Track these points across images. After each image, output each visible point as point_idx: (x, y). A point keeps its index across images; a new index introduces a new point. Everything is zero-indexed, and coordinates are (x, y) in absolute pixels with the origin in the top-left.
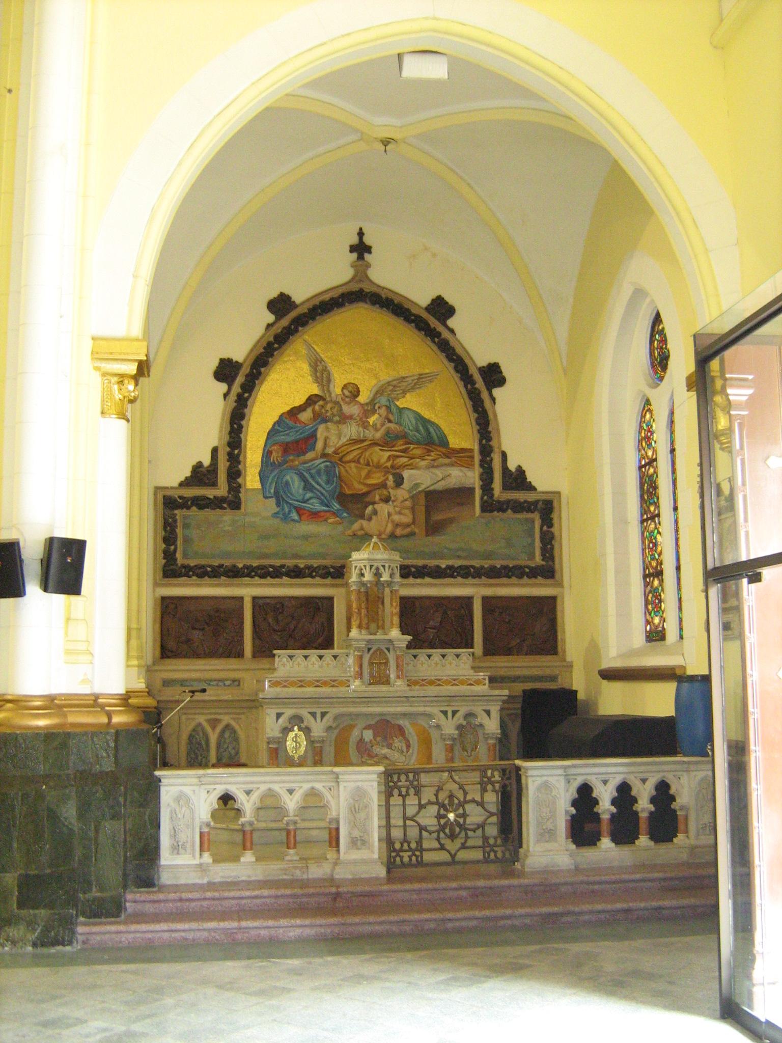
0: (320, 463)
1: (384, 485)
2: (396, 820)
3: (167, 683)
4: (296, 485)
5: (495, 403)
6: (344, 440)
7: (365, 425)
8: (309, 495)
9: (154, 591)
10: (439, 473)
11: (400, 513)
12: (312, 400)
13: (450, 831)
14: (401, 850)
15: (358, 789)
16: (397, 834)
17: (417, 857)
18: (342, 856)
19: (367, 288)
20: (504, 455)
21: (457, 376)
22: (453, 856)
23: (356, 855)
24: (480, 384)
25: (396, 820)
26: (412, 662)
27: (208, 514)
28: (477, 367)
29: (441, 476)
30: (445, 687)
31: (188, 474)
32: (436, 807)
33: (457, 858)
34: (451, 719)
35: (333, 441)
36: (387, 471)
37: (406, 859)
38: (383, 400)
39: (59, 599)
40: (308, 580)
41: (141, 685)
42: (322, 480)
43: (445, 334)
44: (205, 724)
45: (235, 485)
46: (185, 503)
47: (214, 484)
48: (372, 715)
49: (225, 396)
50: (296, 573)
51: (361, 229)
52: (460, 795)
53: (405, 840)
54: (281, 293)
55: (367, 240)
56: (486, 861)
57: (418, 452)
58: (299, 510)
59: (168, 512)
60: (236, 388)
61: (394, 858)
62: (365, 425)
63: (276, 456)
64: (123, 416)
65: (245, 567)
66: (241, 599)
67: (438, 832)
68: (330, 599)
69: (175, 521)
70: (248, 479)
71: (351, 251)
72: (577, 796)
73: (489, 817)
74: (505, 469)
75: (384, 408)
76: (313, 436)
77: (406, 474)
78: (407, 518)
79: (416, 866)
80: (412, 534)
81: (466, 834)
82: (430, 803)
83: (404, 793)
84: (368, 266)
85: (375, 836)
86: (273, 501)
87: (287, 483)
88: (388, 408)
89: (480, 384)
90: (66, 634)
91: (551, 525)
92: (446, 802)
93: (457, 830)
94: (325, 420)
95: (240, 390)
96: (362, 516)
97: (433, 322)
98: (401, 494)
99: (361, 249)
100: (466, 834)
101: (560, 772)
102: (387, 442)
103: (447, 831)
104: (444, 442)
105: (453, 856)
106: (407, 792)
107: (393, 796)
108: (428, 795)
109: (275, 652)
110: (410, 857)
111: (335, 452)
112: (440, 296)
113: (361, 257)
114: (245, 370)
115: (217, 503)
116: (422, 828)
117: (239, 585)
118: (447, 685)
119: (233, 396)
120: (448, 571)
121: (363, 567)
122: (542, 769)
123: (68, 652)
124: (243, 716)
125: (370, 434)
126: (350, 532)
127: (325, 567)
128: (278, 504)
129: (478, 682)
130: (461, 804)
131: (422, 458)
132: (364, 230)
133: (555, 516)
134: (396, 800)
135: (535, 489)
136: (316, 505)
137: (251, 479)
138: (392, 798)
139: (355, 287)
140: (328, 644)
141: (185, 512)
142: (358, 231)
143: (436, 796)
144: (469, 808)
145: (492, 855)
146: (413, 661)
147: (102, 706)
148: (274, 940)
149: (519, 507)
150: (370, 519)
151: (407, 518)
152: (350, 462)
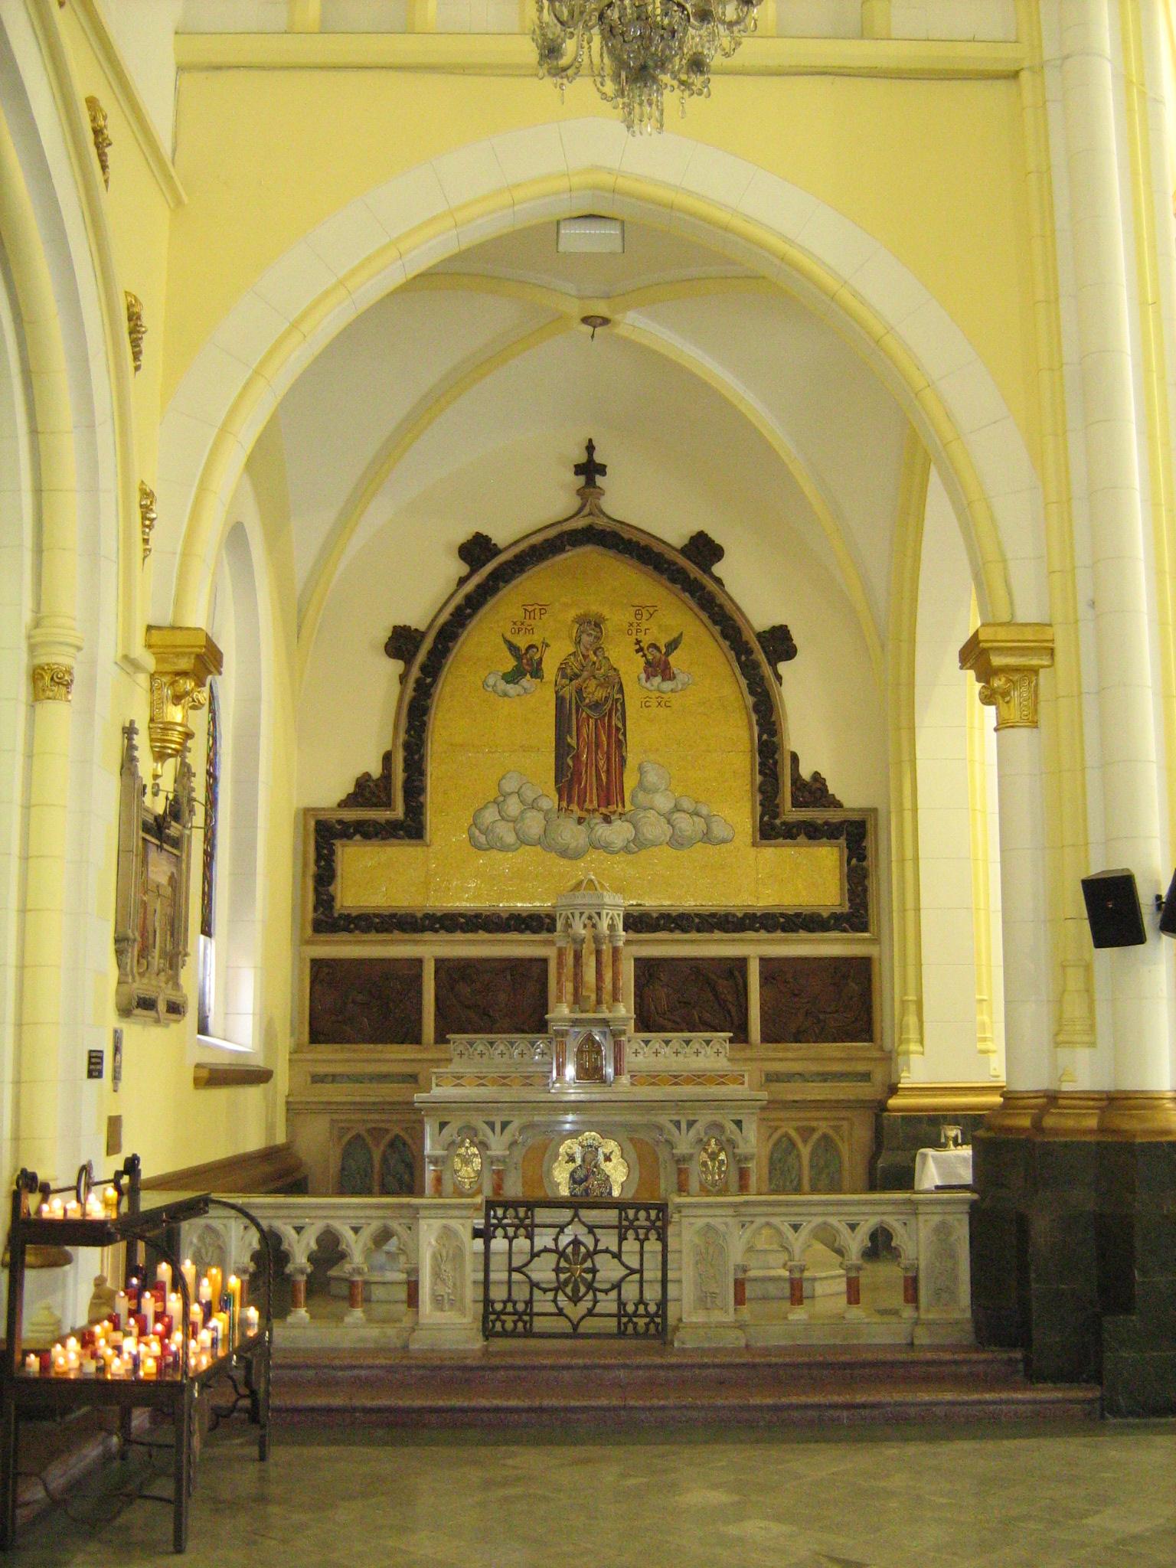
13: (573, 1291)
14: (635, 1314)
16: (498, 1293)
17: (525, 1323)
19: (601, 523)
20: (795, 758)
21: (454, 646)
22: (575, 1327)
26: (466, 1053)
28: (754, 633)
30: (731, 1086)
31: (351, 789)
32: (554, 1257)
33: (581, 1330)
34: (685, 1132)
37: (509, 1326)
44: (793, 1134)
45: (414, 804)
47: (388, 804)
51: (590, 441)
52: (589, 1241)
53: (641, 1301)
55: (598, 458)
56: (621, 1334)
61: (625, 1324)
66: (419, 962)
67: (556, 1290)
68: (544, 961)
71: (576, 473)
72: (869, 1245)
73: (630, 1274)
74: (796, 778)
79: (520, 1336)
81: (595, 1295)
82: (546, 1250)
83: (642, 1237)
84: (601, 492)
85: (471, 1294)
91: (862, 858)
92: (569, 1250)
93: (583, 1289)
97: (694, 571)
99: (590, 470)
100: (595, 1295)
101: (731, 1212)
103: (569, 1290)
105: (575, 1327)
106: (647, 1235)
107: (626, 1239)
109: (448, 1036)
110: (515, 1322)
112: (702, 531)
113: (590, 482)
116: (534, 1285)
117: (416, 942)
118: (733, 1083)
120: (342, 922)
121: (571, 917)
122: (718, 1207)
124: (845, 1124)
129: (739, 1079)
130: (590, 1255)
132: (595, 443)
133: (868, 843)
135: (841, 806)
138: (624, 1243)
139: (580, 523)
140: (542, 1027)
142: (586, 443)
143: (556, 1240)
144: (600, 1259)
145: (498, 1325)
146: (642, 1048)
149: (814, 832)
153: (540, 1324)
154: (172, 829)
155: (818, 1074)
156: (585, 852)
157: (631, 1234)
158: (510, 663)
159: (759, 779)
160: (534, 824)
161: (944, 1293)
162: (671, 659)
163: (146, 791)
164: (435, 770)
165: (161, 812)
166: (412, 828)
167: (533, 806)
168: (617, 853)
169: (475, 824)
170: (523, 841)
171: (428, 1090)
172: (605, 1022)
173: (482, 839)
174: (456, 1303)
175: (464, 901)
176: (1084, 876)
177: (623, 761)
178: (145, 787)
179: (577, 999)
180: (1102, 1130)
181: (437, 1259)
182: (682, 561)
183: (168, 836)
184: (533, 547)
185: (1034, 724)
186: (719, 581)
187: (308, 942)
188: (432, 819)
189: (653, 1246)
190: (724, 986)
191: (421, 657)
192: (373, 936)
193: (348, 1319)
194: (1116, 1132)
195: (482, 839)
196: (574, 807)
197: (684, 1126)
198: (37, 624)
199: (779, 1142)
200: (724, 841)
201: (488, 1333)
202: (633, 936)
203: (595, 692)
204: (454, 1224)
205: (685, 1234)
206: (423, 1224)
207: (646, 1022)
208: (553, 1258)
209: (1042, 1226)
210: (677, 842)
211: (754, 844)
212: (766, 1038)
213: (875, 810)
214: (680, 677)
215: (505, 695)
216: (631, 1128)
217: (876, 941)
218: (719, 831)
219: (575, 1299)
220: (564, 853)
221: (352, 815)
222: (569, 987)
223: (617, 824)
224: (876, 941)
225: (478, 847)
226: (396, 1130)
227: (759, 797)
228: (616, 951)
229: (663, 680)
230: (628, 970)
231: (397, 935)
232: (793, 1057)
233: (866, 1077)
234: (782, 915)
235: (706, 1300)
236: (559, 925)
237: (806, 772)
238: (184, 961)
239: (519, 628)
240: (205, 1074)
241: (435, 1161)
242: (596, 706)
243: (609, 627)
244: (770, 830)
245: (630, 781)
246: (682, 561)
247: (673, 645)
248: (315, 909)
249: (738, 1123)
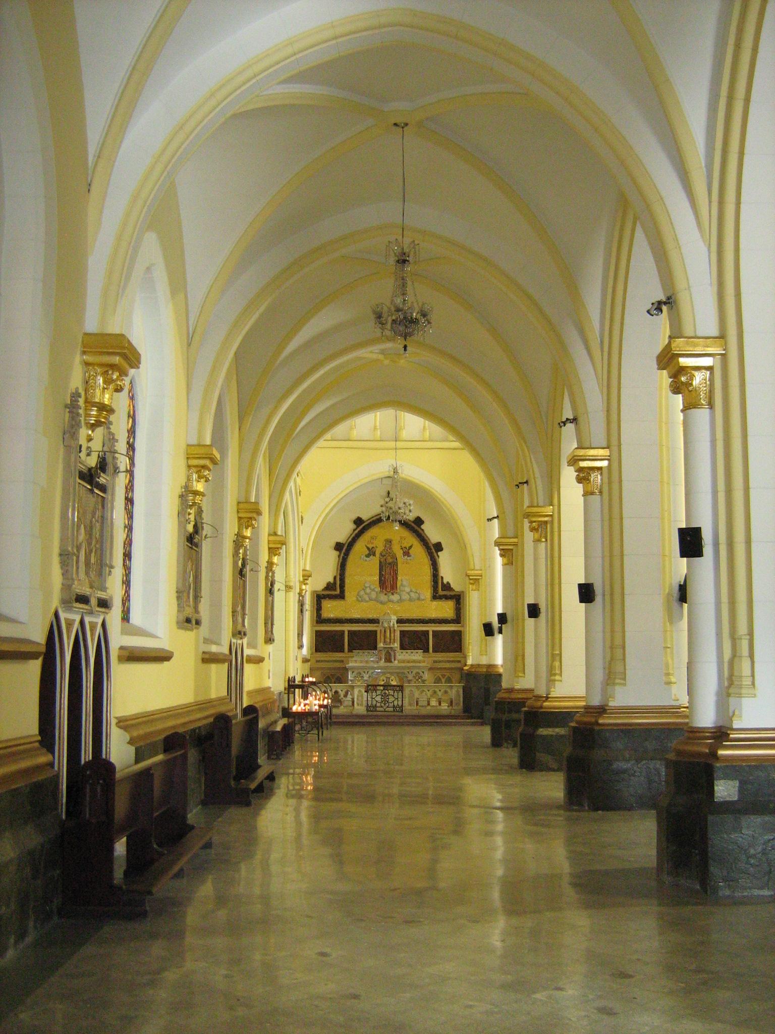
15: (434, 690)
20: (442, 578)
22: (385, 710)
44: (440, 676)
47: (335, 590)
56: (394, 711)
66: (344, 631)
68: (376, 631)
79: (374, 711)
82: (379, 695)
91: (459, 605)
97: (416, 527)
105: (385, 710)
117: (343, 626)
133: (461, 601)
135: (454, 590)
140: (375, 648)
144: (390, 697)
148: (273, 739)
149: (447, 598)
153: (378, 709)
154: (101, 478)
155: (448, 661)
156: (387, 602)
157: (396, 691)
158: (367, 552)
159: (432, 583)
160: (373, 595)
161: (458, 704)
162: (410, 551)
163: (82, 449)
164: (347, 581)
165: (93, 465)
166: (341, 596)
167: (373, 590)
168: (395, 603)
169: (358, 595)
170: (371, 600)
171: (349, 664)
172: (392, 648)
173: (360, 599)
174: (362, 705)
175: (356, 615)
176: (484, 622)
177: (397, 578)
178: (81, 446)
179: (385, 642)
180: (487, 672)
181: (358, 696)
182: (413, 525)
183: (98, 483)
184: (373, 521)
185: (479, 590)
186: (423, 530)
187: (315, 626)
188: (347, 594)
189: (400, 693)
190: (423, 638)
191: (344, 550)
192: (332, 625)
193: (340, 708)
194: (489, 672)
195: (360, 599)
196: (384, 590)
198: (286, 577)
199: (436, 679)
200: (423, 600)
202: (399, 624)
203: (390, 560)
204: (361, 689)
205: (407, 692)
206: (355, 689)
207: (403, 647)
208: (380, 696)
209: (474, 690)
210: (411, 600)
211: (431, 600)
212: (434, 651)
213: (463, 592)
214: (412, 556)
215: (366, 560)
216: (398, 673)
217: (463, 626)
218: (422, 597)
219: (385, 693)
220: (382, 603)
222: (382, 638)
223: (395, 595)
224: (463, 626)
225: (359, 601)
226: (339, 675)
227: (432, 588)
228: (394, 630)
229: (408, 556)
230: (398, 634)
231: (338, 624)
232: (440, 656)
233: (459, 662)
234: (438, 619)
235: (410, 704)
236: (380, 623)
237: (445, 582)
238: (200, 600)
239: (369, 542)
240: (305, 660)
241: (351, 681)
242: (390, 564)
243: (394, 542)
244: (435, 597)
245: (399, 584)
246: (413, 525)
247: (411, 547)
248: (317, 617)
249: (423, 672)
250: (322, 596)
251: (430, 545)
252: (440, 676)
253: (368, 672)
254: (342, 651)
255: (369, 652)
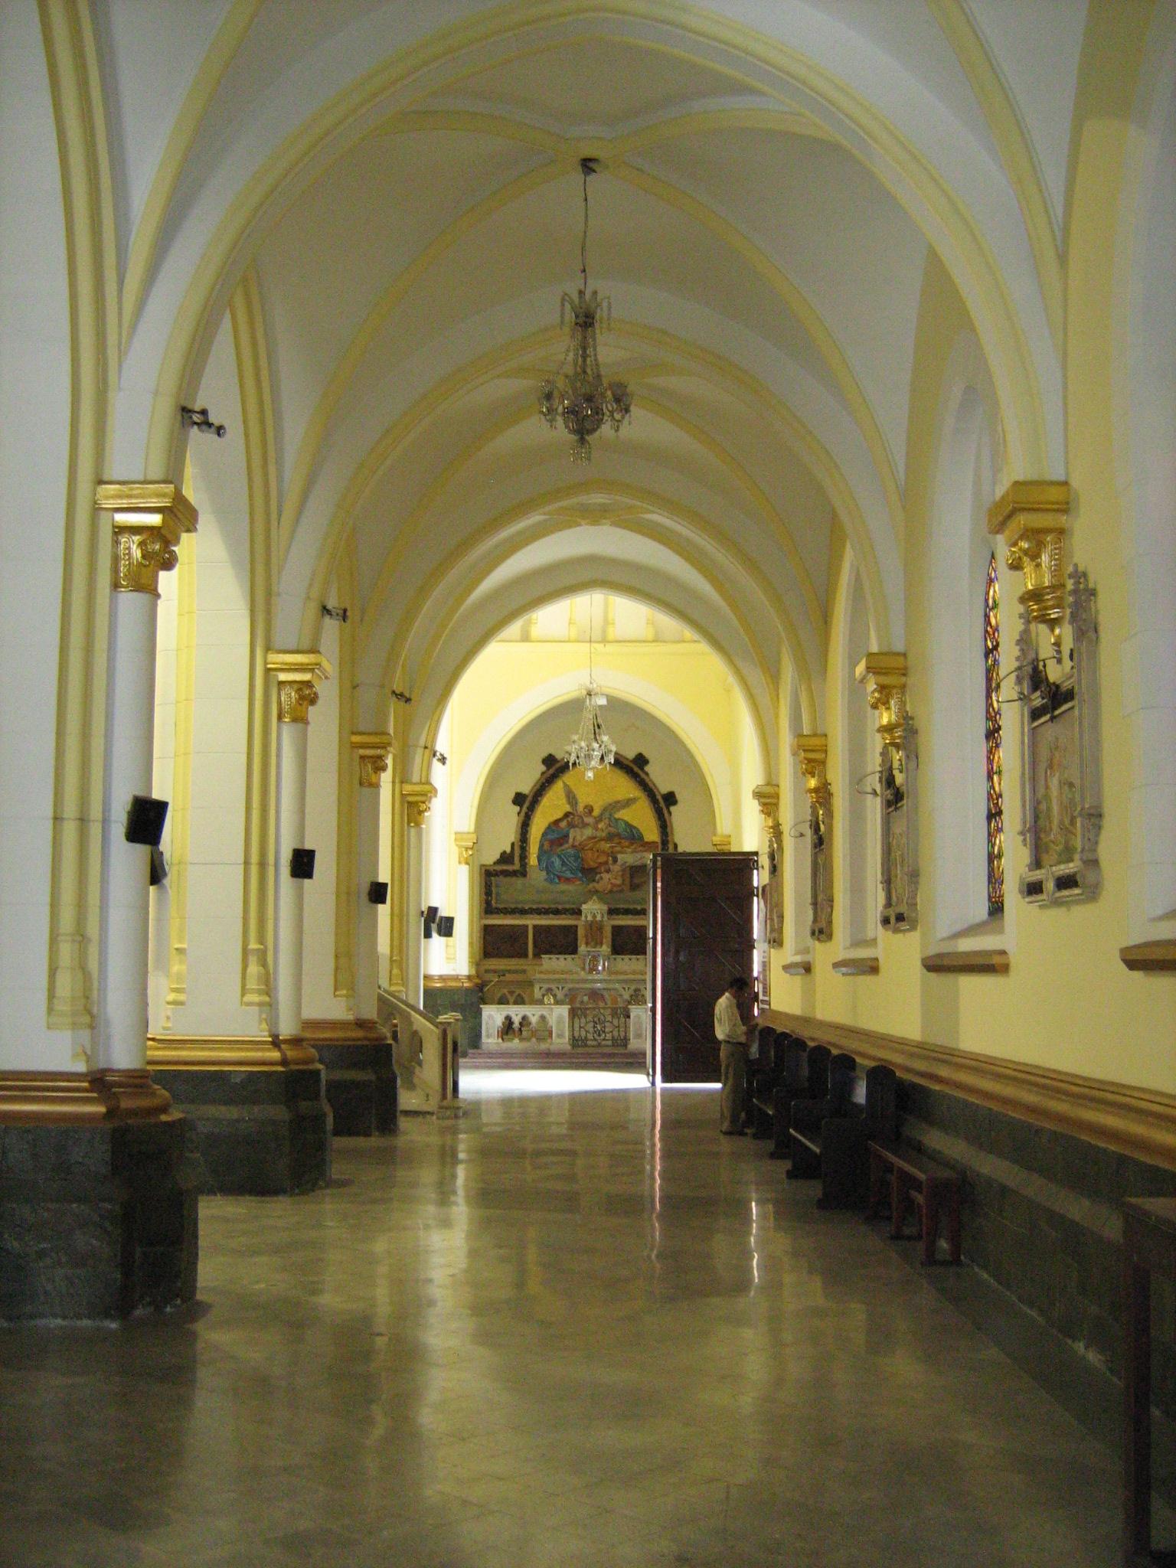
0: (571, 851)
1: (606, 863)
2: (577, 1028)
3: (487, 971)
4: (557, 863)
5: (671, 815)
6: (584, 837)
7: (597, 829)
8: (564, 869)
9: (480, 922)
10: (639, 856)
11: (615, 879)
12: (567, 815)
18: (554, 1041)
23: (558, 1041)
24: (662, 804)
25: (577, 1028)
27: (508, 879)
29: (639, 857)
35: (578, 838)
36: (608, 855)
38: (607, 815)
39: (444, 939)
40: (564, 916)
41: (473, 972)
42: (572, 859)
43: (643, 776)
44: (507, 993)
46: (497, 874)
48: (587, 989)
49: (519, 814)
50: (557, 912)
54: (550, 755)
57: (627, 844)
58: (559, 878)
59: (488, 878)
60: (525, 809)
62: (597, 829)
63: (546, 846)
64: (467, 863)
65: (530, 908)
66: (527, 926)
68: (577, 927)
69: (491, 884)
70: (531, 860)
71: (1020, 618)
75: (607, 820)
76: (567, 836)
77: (619, 856)
78: (619, 882)
80: (621, 891)
85: (567, 1034)
86: (544, 873)
87: (553, 862)
88: (610, 819)
89: (662, 804)
90: (447, 952)
94: (574, 826)
95: (527, 811)
96: (594, 881)
97: (636, 769)
98: (616, 868)
102: (610, 837)
104: (641, 837)
108: (590, 1018)
111: (580, 845)
114: (529, 799)
115: (514, 873)
119: (523, 814)
123: (448, 958)
125: (599, 834)
126: (586, 890)
127: (573, 909)
128: (547, 874)
131: (628, 847)
134: (576, 1020)
136: (568, 875)
137: (533, 860)
140: (574, 951)
141: (497, 878)
147: (460, 979)
150: (598, 882)
151: (619, 882)
152: (587, 850)
153: (589, 1043)
197: (560, 988)
201: (574, 1046)
221: (499, 868)
236: (583, 915)
250: (494, 872)
251: (659, 797)
252: (507, 993)
253: (562, 988)
254: (524, 955)
255: (558, 959)
